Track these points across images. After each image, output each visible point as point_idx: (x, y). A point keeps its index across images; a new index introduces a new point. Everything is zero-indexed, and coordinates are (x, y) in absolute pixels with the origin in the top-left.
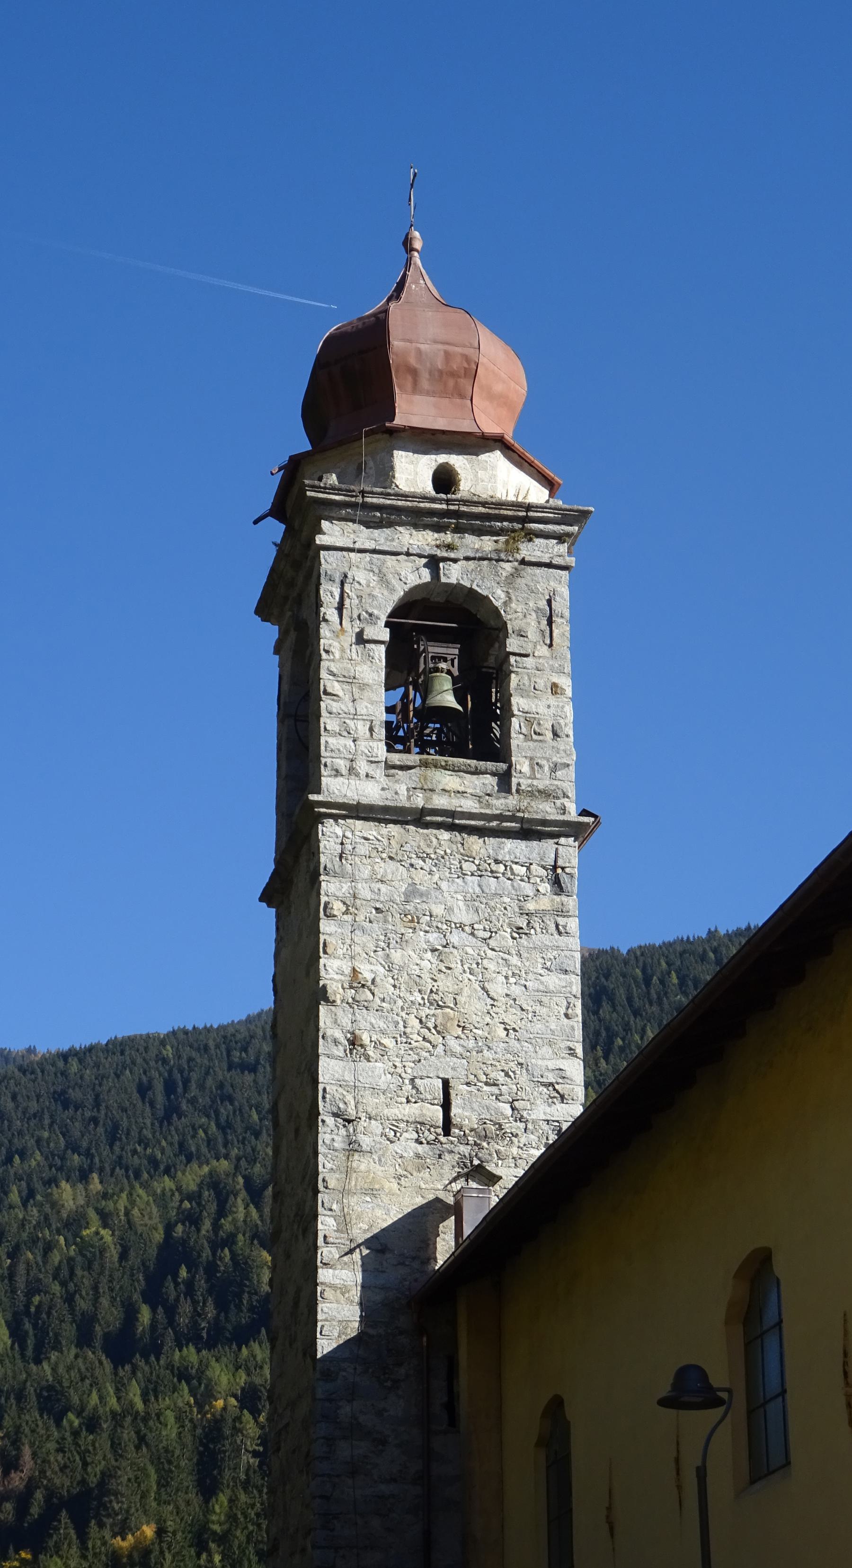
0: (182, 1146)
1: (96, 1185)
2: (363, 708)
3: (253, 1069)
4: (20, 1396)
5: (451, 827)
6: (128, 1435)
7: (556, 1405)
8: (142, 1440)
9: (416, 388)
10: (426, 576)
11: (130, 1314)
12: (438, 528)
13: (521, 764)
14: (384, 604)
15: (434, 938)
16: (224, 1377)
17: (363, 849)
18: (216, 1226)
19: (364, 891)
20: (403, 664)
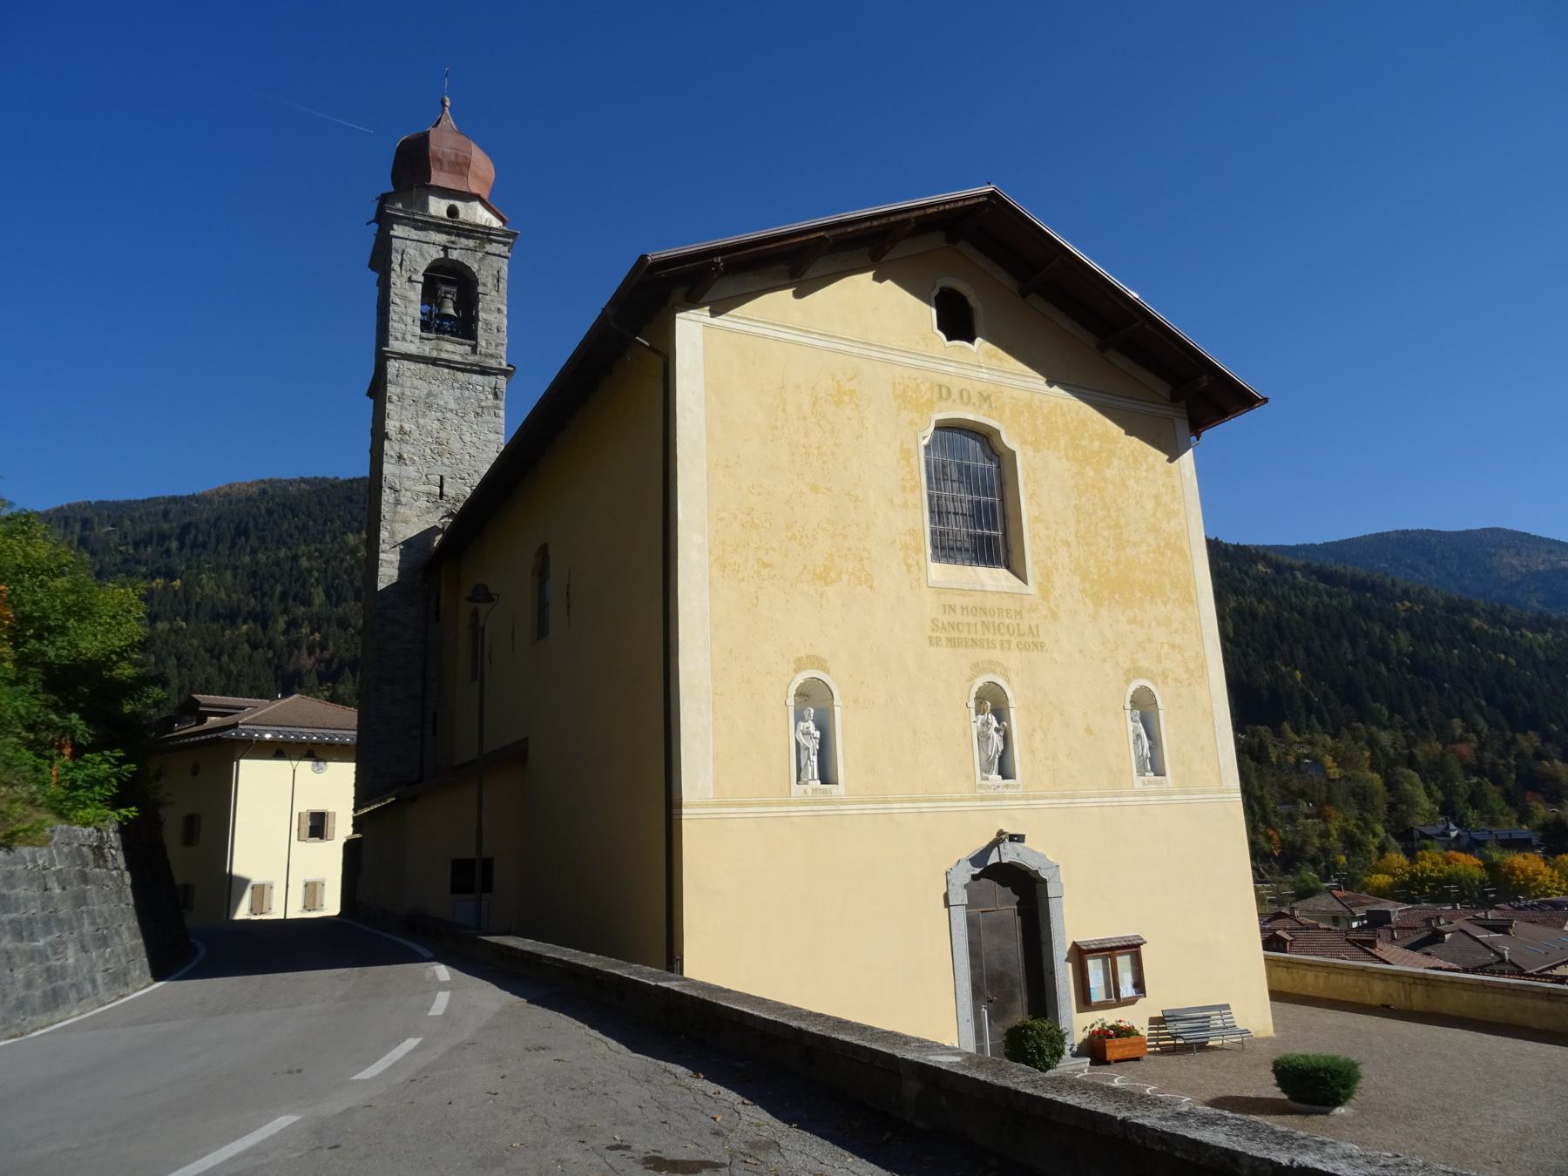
2: (410, 311)
4: (329, 620)
9: (441, 169)
10: (442, 255)
12: (449, 234)
13: (482, 343)
17: (408, 373)
19: (407, 392)
20: (430, 293)
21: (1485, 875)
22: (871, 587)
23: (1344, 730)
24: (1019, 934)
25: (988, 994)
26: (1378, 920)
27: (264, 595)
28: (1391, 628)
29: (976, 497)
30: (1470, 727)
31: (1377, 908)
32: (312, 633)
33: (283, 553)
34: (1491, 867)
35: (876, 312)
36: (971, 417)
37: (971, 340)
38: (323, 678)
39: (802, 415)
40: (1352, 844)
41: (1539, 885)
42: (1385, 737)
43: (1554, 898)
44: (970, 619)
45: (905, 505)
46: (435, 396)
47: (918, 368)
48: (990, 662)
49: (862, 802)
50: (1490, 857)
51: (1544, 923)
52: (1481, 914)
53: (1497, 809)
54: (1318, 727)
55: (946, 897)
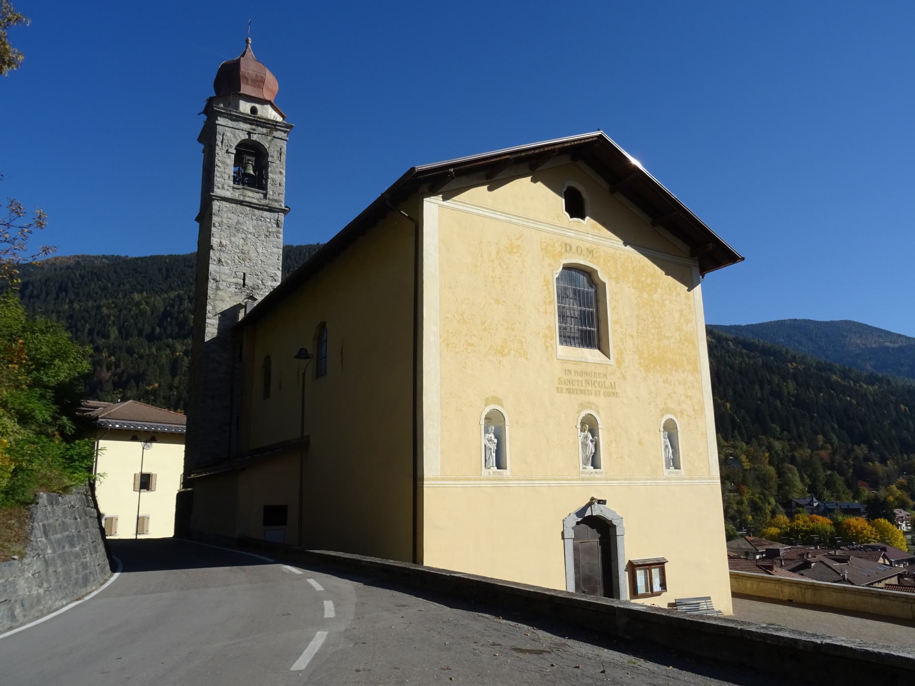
0: (170, 286)
1: (145, 294)
2: (227, 171)
3: (191, 267)
4: (121, 348)
5: (250, 206)
6: (151, 360)
7: (268, 357)
8: (155, 362)
9: (247, 84)
10: (247, 137)
11: (153, 329)
12: (251, 124)
14: (235, 143)
15: (243, 235)
16: (180, 348)
17: (225, 209)
18: (179, 308)
19: (225, 221)
21: (833, 529)
22: (527, 358)
23: (754, 440)
24: (600, 555)
25: (582, 587)
26: (772, 554)
27: (77, 330)
28: (784, 379)
29: (583, 308)
30: (828, 440)
31: (771, 547)
32: (109, 356)
33: (90, 303)
34: (837, 524)
35: (532, 202)
36: (582, 262)
37: (583, 218)
38: (116, 385)
39: (491, 257)
40: (756, 508)
41: (864, 536)
42: (777, 445)
43: (872, 544)
44: (579, 378)
45: (546, 312)
46: (241, 224)
47: (554, 233)
48: (589, 403)
49: (519, 480)
50: (837, 519)
51: (867, 558)
52: (832, 552)
53: (841, 490)
54: (738, 437)
55: (563, 533)
